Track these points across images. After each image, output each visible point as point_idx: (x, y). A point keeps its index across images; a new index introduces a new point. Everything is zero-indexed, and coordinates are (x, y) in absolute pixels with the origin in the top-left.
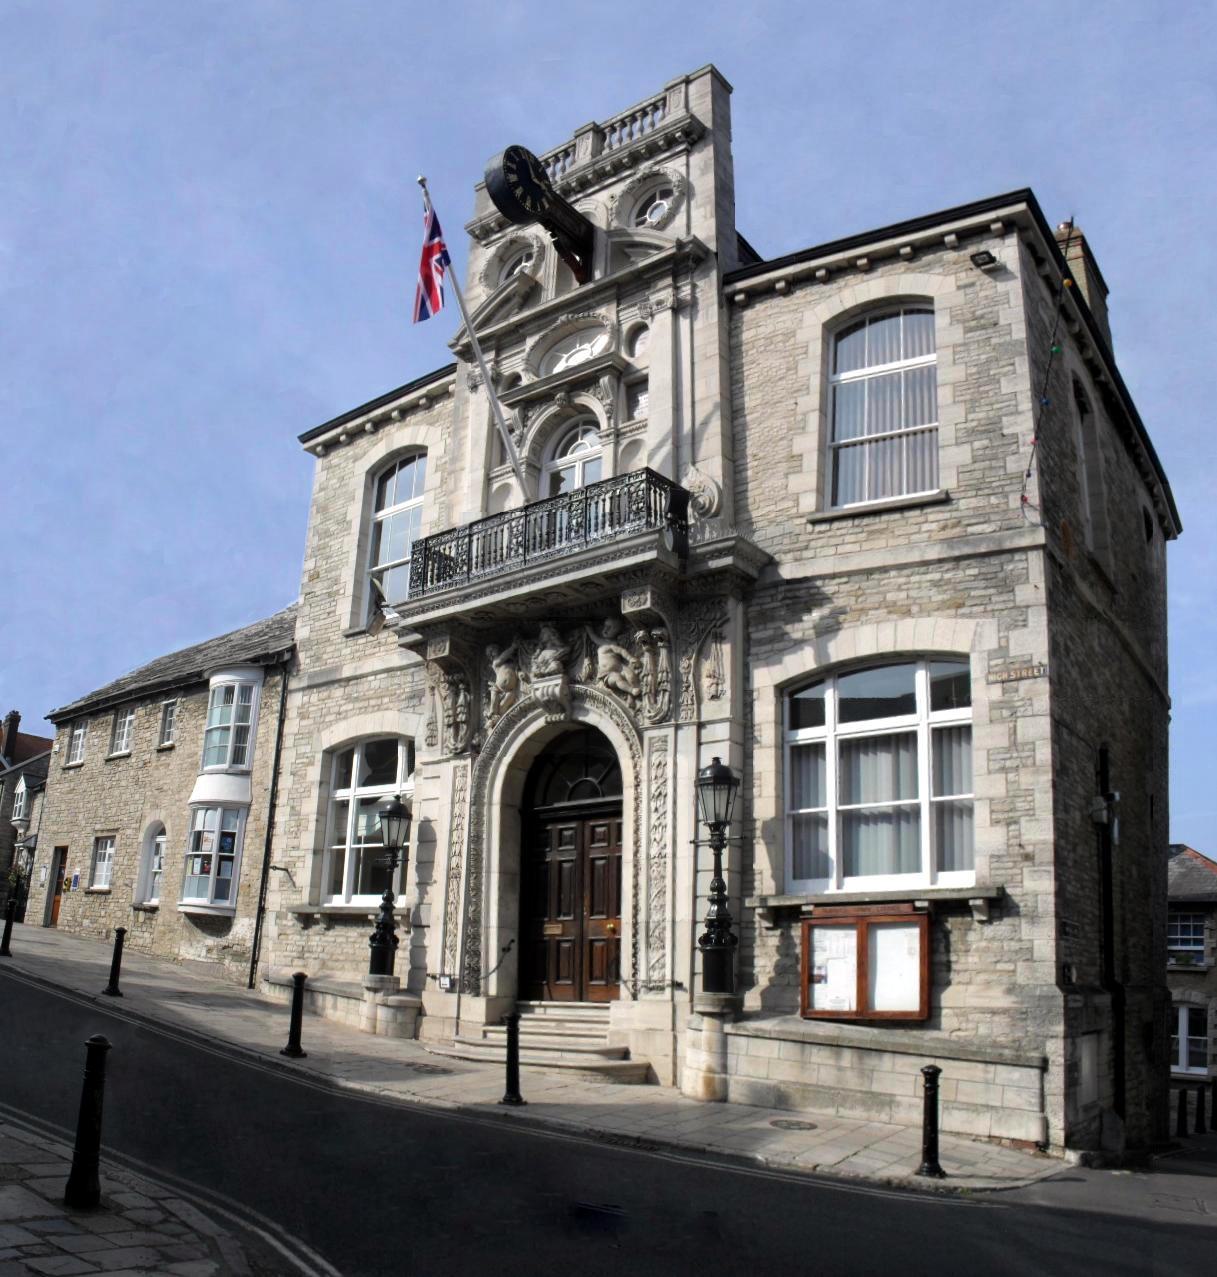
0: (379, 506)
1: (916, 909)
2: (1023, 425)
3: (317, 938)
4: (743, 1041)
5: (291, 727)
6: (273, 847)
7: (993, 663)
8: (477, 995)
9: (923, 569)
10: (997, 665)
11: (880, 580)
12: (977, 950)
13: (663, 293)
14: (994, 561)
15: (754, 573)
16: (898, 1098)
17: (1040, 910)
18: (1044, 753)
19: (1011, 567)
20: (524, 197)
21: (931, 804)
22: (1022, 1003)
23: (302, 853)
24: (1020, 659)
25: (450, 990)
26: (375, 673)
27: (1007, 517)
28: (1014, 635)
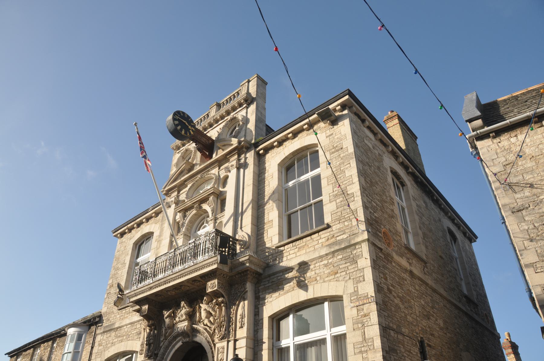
0: (137, 257)
5: (95, 350)
7: (352, 298)
9: (320, 260)
11: (304, 268)
13: (233, 161)
14: (349, 250)
18: (378, 343)
19: (355, 252)
24: (363, 295)
26: (126, 325)
28: (360, 285)
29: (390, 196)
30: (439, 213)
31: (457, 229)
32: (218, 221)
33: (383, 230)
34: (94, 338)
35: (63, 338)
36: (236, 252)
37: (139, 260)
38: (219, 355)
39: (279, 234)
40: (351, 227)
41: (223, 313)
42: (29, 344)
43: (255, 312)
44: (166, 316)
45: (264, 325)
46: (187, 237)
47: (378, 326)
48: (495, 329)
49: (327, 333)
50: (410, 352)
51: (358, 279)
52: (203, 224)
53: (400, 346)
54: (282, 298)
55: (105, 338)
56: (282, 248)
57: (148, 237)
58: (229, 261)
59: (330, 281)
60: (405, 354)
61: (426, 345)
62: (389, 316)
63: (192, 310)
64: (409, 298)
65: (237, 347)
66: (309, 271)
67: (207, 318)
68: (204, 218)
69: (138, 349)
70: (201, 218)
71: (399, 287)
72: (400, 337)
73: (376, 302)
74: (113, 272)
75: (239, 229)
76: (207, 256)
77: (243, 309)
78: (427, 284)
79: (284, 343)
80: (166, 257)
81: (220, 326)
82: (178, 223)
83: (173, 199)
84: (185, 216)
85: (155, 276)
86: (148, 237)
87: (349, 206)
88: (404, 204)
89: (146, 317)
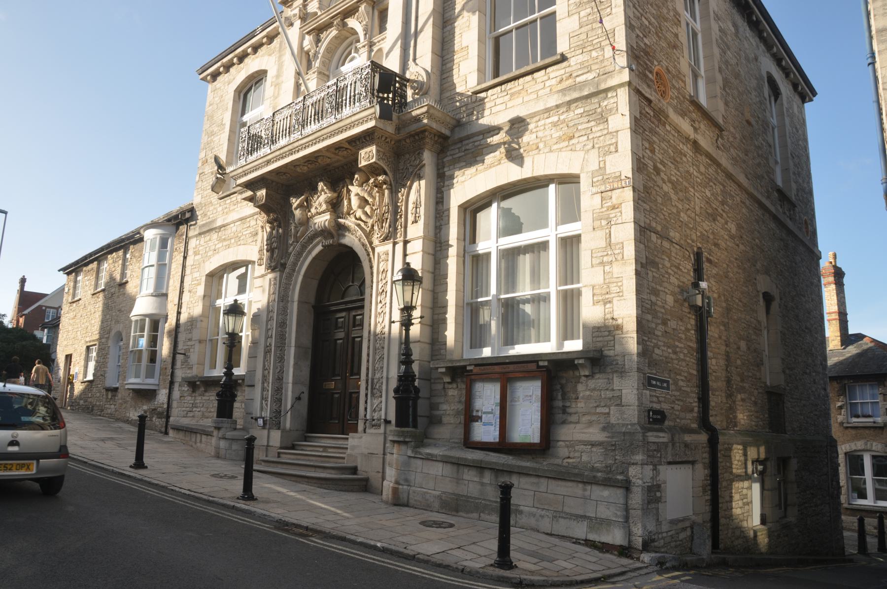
1: (538, 367)
4: (419, 462)
5: (189, 262)
7: (595, 180)
8: (279, 429)
9: (546, 115)
11: (518, 128)
12: (583, 398)
14: (595, 100)
15: (446, 132)
16: (522, 508)
17: (627, 367)
18: (630, 251)
19: (605, 103)
21: (558, 292)
22: (612, 437)
23: (193, 343)
24: (613, 175)
25: (264, 427)
26: (234, 222)
28: (609, 158)
29: (675, 10)
30: (757, 46)
31: (784, 76)
32: (375, 49)
33: (656, 69)
34: (186, 244)
35: (138, 246)
36: (406, 100)
37: (246, 118)
38: (381, 265)
39: (479, 70)
40: (602, 61)
41: (386, 199)
42: (90, 255)
43: (437, 198)
44: (294, 206)
45: (451, 219)
46: (324, 76)
47: (632, 224)
48: (815, 244)
49: (551, 233)
50: (678, 268)
51: (606, 149)
52: (350, 53)
53: (664, 257)
54: (481, 176)
55: (202, 242)
56: (483, 95)
57: (257, 79)
58: (395, 115)
59: (561, 149)
60: (670, 271)
61: (704, 259)
62: (651, 211)
63: (335, 195)
64: (687, 185)
65: (408, 252)
66: (527, 133)
67: (361, 207)
68: (351, 44)
69: (255, 257)
70: (346, 43)
71: (673, 166)
72: (666, 244)
73: (633, 187)
74: (205, 139)
75: (411, 62)
76: (357, 107)
77: (418, 193)
78: (719, 165)
79: (482, 247)
80: (290, 111)
81: (381, 221)
82: (307, 53)
83: (297, 11)
84: (318, 41)
85: (273, 142)
86: (257, 79)
87: (601, 22)
88: (698, 26)
89: (265, 208)
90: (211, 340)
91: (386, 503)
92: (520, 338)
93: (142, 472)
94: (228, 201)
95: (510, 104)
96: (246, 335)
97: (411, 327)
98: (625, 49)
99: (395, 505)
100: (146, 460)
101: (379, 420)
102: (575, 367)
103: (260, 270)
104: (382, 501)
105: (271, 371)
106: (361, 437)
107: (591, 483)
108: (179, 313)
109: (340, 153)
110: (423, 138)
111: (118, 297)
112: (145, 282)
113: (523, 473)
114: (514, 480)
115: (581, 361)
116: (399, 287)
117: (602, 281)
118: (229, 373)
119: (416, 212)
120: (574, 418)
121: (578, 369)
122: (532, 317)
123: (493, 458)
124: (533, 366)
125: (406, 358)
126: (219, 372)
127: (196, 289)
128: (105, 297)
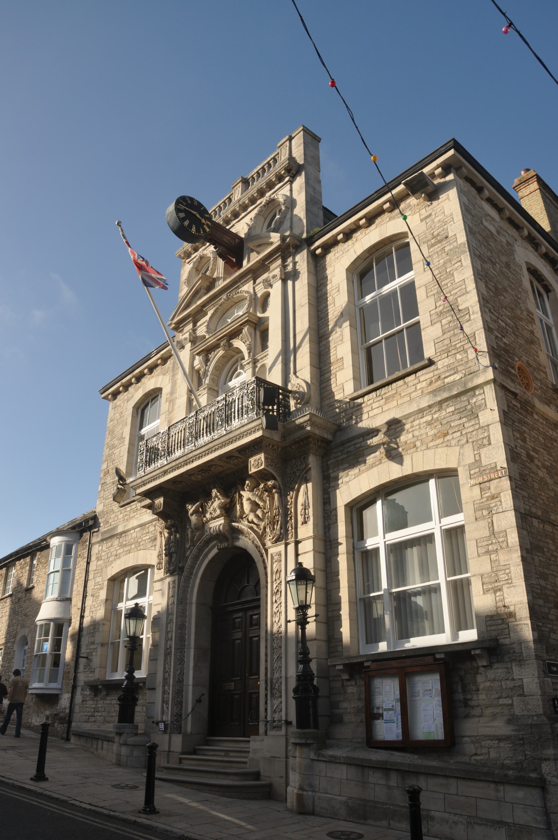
0: (141, 427)
1: (436, 660)
2: (470, 301)
3: (101, 702)
4: (323, 765)
5: (92, 567)
6: (82, 643)
7: (472, 472)
8: (180, 733)
9: (420, 415)
10: (475, 473)
11: (395, 429)
13: (275, 269)
14: (464, 398)
15: (329, 437)
16: (433, 813)
17: (524, 654)
18: (513, 538)
19: (474, 400)
20: (190, 226)
21: (448, 583)
24: (489, 467)
25: (165, 732)
26: (134, 528)
27: (468, 366)
28: (483, 451)
29: (528, 310)
32: (259, 365)
33: (517, 365)
35: (44, 552)
36: (289, 409)
37: (144, 431)
38: (275, 565)
39: (354, 378)
40: (467, 362)
43: (324, 498)
44: (191, 512)
46: (213, 391)
47: (513, 513)
49: (435, 526)
55: (104, 548)
56: (360, 401)
57: (154, 395)
58: (280, 425)
63: (228, 500)
65: (300, 552)
67: (253, 511)
69: (154, 561)
70: (232, 362)
71: (545, 452)
72: (548, 528)
74: (106, 452)
75: (292, 375)
77: (305, 495)
79: (370, 543)
80: (184, 425)
81: (273, 523)
82: (198, 371)
83: (187, 335)
84: (207, 361)
85: (169, 453)
86: (154, 395)
87: (462, 329)
88: (551, 321)
89: (162, 515)
90: (113, 643)
91: (291, 811)
92: (415, 631)
93: (43, 784)
94: (128, 509)
95: (385, 408)
96: (147, 638)
97: (307, 626)
98: (486, 350)
99: (301, 813)
100: (48, 771)
101: (280, 721)
102: (473, 658)
103: (159, 574)
104: (287, 810)
105: (172, 674)
106: (263, 740)
107: (503, 783)
108: (82, 617)
109: (231, 462)
110: (309, 444)
111: (25, 602)
112: (50, 587)
113: (430, 773)
114: (422, 783)
115: (478, 652)
116: (293, 587)
117: (490, 570)
118: (130, 677)
119: (305, 514)
120: (477, 712)
121: (475, 660)
122: (424, 610)
123: (398, 757)
124: (429, 659)
125: (304, 657)
126: (120, 675)
127: (99, 593)
128: (12, 602)
